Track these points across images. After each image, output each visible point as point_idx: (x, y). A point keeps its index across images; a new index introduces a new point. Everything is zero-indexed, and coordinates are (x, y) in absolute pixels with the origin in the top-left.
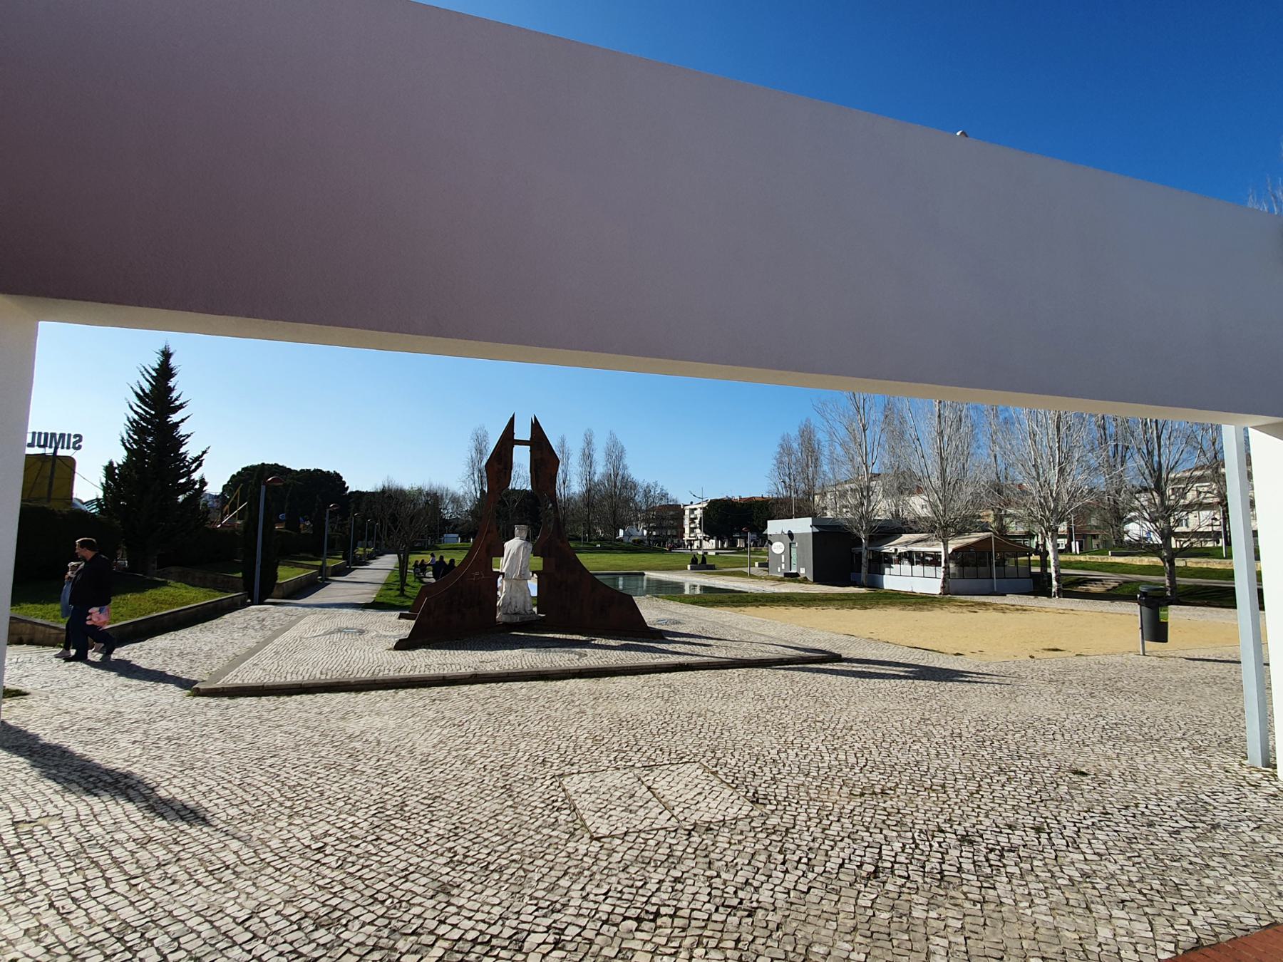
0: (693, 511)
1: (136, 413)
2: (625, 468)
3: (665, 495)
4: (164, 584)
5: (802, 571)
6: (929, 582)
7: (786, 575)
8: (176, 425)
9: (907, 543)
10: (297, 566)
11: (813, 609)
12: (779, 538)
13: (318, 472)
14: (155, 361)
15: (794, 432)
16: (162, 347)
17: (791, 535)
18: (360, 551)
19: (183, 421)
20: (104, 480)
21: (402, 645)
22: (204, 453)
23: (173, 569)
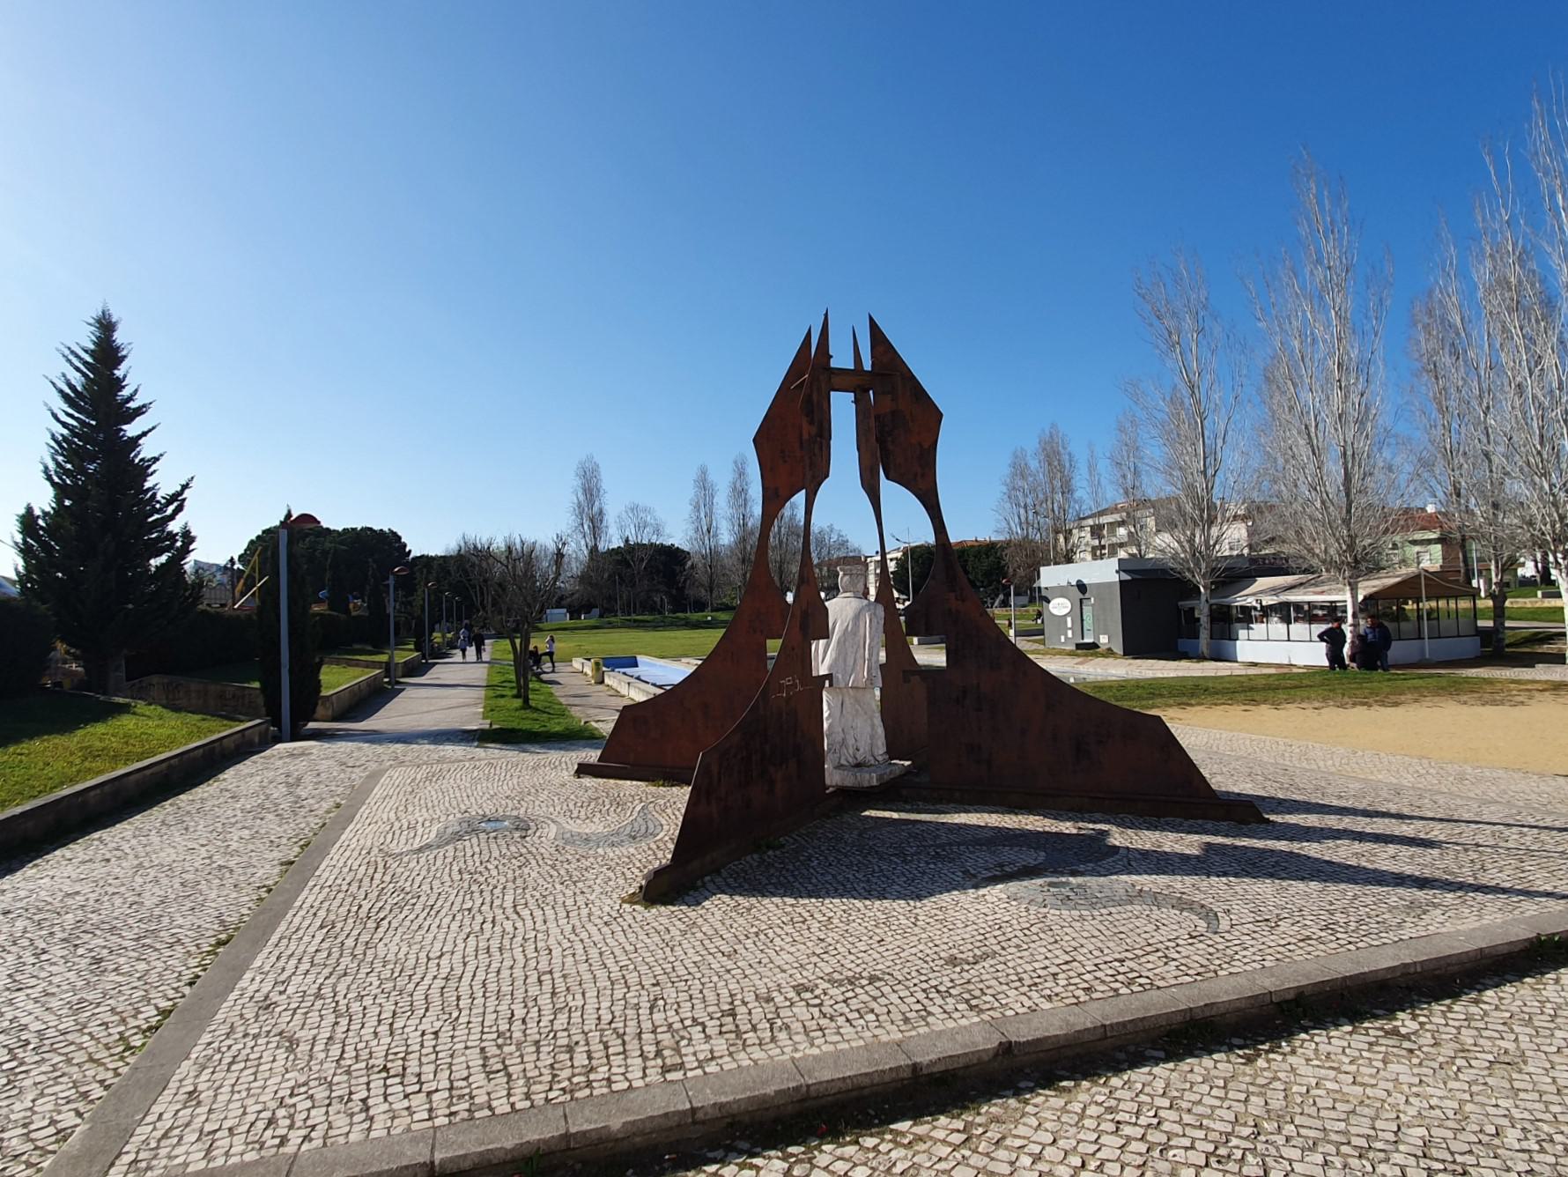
1: (65, 425)
3: (844, 544)
4: (124, 709)
5: (1104, 639)
6: (1303, 649)
7: (1079, 646)
8: (134, 442)
9: (1275, 591)
10: (350, 663)
11: (1264, 709)
12: (1061, 592)
13: (368, 530)
14: (85, 338)
15: (1031, 445)
16: (97, 313)
17: (1082, 587)
18: (437, 637)
19: (144, 434)
20: (19, 538)
21: (666, 888)
22: (185, 487)
23: (155, 679)
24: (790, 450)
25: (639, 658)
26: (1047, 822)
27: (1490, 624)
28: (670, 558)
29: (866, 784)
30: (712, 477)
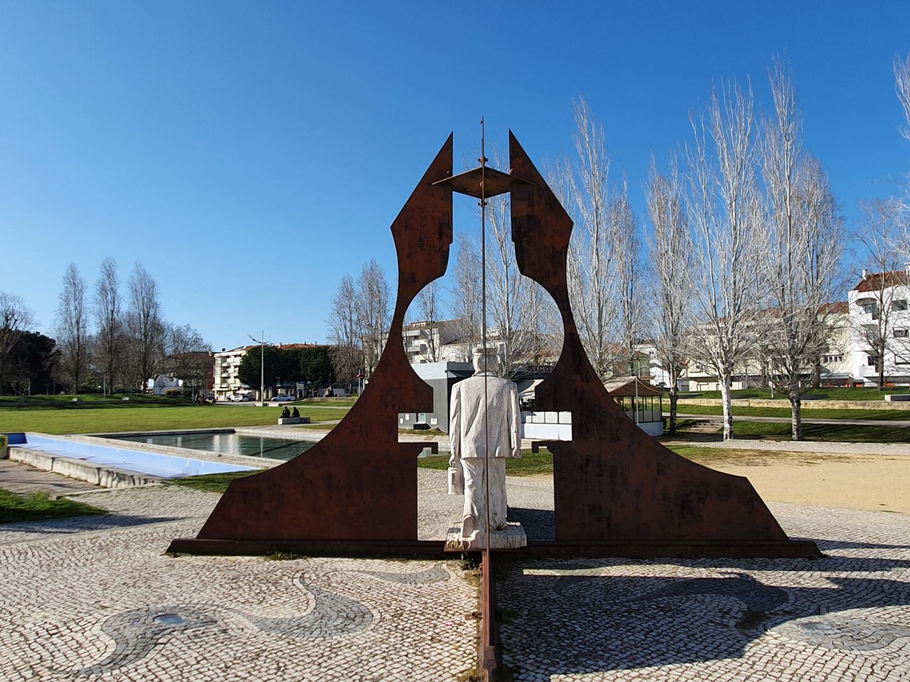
0: (225, 358)
2: (156, 306)
3: (197, 341)
7: (416, 427)
15: (357, 276)
24: (422, 245)
25: (28, 435)
26: (688, 570)
27: (668, 414)
28: (38, 345)
29: (517, 546)
30: (82, 274)
